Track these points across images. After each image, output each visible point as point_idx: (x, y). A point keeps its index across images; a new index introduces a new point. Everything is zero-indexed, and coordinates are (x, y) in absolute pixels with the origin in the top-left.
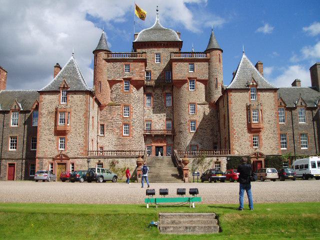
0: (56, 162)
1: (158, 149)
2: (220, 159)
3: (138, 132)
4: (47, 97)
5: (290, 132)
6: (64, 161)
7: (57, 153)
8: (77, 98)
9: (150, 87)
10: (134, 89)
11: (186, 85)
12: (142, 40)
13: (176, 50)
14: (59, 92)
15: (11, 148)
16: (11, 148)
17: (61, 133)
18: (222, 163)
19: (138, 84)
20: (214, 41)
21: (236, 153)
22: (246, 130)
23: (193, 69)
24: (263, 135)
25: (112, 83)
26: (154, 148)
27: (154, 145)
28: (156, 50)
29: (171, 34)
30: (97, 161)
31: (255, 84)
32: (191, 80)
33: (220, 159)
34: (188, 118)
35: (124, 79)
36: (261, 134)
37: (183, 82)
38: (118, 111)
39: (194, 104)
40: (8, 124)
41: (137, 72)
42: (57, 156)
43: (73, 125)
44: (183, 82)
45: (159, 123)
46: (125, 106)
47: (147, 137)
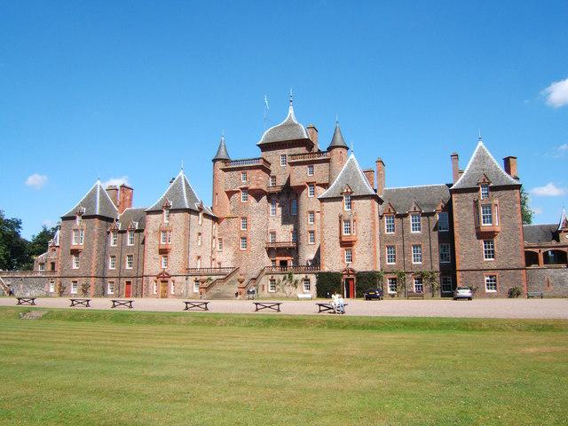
0: (159, 280)
1: (284, 264)
2: (310, 276)
3: (257, 245)
4: (153, 217)
5: (398, 244)
6: (166, 279)
7: (160, 271)
8: (178, 216)
9: (274, 194)
10: (252, 200)
11: (305, 192)
12: (267, 142)
13: (302, 150)
14: (162, 211)
15: (484, 222)
16: (484, 222)
17: (164, 252)
18: (311, 280)
19: (258, 194)
20: (338, 136)
21: (326, 269)
22: (338, 244)
23: (312, 172)
24: (356, 248)
25: (230, 194)
26: (278, 263)
27: (279, 259)
28: (281, 152)
29: (299, 130)
30: (194, 278)
31: (349, 190)
32: (311, 184)
33: (310, 276)
34: (307, 229)
35: (241, 189)
36: (354, 247)
37: (303, 188)
38: (236, 224)
39: (312, 213)
40: (126, 243)
41: (258, 180)
42: (160, 274)
43: (175, 242)
44: (303, 188)
45: (284, 236)
46: (243, 218)
47: (270, 251)
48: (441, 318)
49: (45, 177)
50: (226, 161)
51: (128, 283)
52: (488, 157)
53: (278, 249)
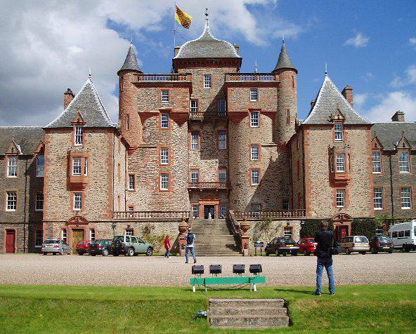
1: (208, 208)
3: (180, 186)
4: (56, 137)
6: (81, 226)
7: (71, 215)
11: (246, 120)
17: (76, 187)
19: (180, 118)
20: (286, 57)
21: (313, 215)
23: (256, 97)
24: (351, 189)
25: (144, 116)
28: (204, 71)
29: (226, 48)
30: (125, 226)
31: (341, 117)
33: (292, 224)
34: (248, 166)
35: (161, 111)
36: (348, 187)
38: (153, 156)
39: (256, 146)
41: (179, 101)
43: (93, 175)
45: (210, 173)
46: (163, 148)
47: (193, 193)
48: (385, 287)
49: (367, 40)
50: (138, 73)
51: (11, 232)
52: (9, 129)
53: (204, 190)
